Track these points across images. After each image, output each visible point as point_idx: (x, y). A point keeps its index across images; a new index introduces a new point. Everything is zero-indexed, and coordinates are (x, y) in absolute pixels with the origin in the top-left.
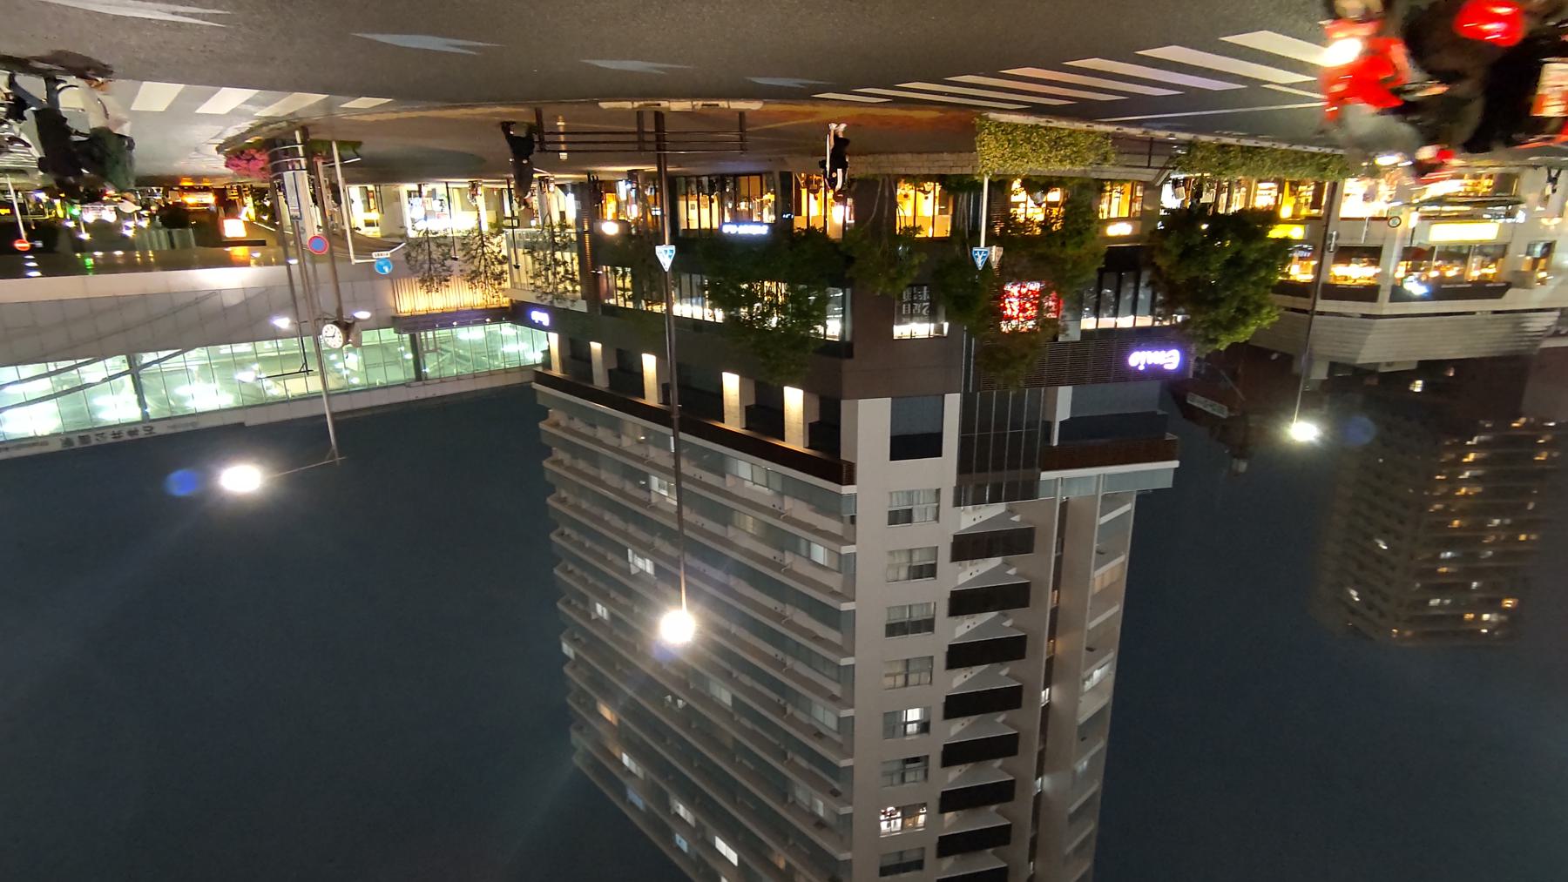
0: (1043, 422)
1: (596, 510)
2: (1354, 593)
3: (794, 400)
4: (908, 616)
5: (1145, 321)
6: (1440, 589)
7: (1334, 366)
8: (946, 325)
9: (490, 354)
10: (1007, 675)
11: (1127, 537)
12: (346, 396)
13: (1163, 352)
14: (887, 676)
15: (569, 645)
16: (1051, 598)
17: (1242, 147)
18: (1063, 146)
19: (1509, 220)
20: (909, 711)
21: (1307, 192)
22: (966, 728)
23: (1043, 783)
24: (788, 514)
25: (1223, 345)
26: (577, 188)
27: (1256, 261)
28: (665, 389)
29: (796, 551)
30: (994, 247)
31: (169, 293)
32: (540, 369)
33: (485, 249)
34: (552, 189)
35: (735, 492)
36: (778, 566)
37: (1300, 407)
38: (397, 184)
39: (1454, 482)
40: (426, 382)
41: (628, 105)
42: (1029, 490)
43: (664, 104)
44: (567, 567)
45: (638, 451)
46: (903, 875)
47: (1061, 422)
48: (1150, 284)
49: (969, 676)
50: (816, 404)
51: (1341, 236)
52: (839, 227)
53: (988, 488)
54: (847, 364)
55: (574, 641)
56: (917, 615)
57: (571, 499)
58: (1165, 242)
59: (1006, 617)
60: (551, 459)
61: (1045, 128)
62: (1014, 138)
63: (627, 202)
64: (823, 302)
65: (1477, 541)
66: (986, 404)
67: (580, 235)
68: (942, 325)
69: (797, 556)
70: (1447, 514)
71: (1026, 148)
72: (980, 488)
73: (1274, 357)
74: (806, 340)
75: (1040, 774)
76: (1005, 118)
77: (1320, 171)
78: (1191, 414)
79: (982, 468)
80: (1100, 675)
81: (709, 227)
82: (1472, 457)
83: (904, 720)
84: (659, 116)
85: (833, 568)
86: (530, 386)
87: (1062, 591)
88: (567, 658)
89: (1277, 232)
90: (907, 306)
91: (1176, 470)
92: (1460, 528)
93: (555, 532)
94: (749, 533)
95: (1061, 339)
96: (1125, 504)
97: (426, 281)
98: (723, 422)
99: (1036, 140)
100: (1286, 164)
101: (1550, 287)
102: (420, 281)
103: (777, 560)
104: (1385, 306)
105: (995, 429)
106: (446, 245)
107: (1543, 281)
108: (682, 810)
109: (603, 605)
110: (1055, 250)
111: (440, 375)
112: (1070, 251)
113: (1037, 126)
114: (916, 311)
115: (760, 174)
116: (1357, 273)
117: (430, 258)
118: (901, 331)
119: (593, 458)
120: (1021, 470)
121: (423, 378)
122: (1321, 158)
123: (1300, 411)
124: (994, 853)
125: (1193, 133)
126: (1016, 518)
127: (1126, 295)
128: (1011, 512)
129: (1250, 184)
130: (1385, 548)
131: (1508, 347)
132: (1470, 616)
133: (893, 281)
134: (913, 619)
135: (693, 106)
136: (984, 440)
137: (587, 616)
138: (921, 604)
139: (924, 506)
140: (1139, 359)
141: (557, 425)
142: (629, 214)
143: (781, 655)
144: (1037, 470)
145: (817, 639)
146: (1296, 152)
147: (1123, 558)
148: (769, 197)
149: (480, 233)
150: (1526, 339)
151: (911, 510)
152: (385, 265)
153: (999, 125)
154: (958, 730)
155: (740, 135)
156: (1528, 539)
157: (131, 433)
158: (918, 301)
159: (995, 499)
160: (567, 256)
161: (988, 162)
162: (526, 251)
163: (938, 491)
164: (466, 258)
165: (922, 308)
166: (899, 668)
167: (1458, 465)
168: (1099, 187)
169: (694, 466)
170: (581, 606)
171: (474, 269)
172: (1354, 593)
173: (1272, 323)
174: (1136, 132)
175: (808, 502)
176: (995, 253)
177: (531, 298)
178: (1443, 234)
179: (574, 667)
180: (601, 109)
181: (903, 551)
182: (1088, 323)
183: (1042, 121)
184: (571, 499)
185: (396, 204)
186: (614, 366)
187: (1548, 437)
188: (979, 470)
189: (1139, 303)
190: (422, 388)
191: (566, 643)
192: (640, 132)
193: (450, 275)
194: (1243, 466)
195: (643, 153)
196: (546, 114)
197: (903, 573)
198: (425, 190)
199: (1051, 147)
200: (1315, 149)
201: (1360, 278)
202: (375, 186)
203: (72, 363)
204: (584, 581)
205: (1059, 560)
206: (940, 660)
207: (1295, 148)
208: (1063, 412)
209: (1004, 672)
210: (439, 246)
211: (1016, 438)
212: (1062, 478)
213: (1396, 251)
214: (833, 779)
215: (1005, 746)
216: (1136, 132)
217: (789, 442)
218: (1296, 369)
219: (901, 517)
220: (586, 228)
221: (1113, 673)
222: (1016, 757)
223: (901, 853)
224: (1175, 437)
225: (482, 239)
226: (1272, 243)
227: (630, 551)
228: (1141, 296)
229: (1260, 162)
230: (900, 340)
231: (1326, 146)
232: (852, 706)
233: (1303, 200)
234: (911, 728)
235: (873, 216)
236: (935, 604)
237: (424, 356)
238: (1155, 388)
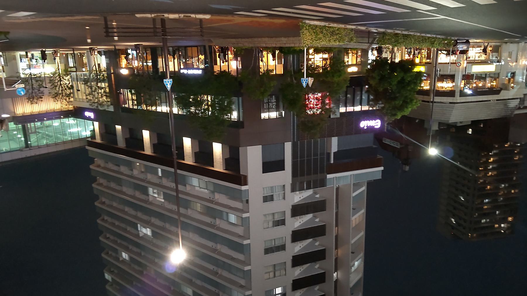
0: (326, 152)
1: (121, 207)
2: (453, 220)
3: (217, 148)
4: (273, 244)
5: (366, 108)
6: (485, 215)
7: (440, 124)
8: (283, 112)
9: (63, 133)
10: (318, 268)
13: (374, 121)
14: (266, 273)
16: (335, 230)
17: (403, 34)
18: (335, 34)
19: (498, 64)
20: (276, 289)
21: (424, 52)
24: (217, 201)
25: (399, 117)
26: (106, 53)
27: (409, 81)
28: (155, 147)
29: (221, 218)
30: (310, 78)
32: (90, 139)
33: (62, 82)
34: (96, 53)
35: (191, 192)
36: (212, 226)
38: (15, 52)
39: (486, 170)
40: (31, 148)
41: (149, 16)
42: (322, 183)
43: (166, 15)
44: (106, 235)
45: (142, 176)
48: (368, 91)
49: (302, 270)
50: (227, 150)
51: (441, 70)
52: (235, 70)
53: (305, 183)
54: (241, 130)
55: (111, 272)
56: (278, 243)
57: (107, 202)
59: (316, 241)
60: (96, 183)
61: (328, 27)
62: (316, 32)
63: (132, 59)
64: (230, 103)
65: (496, 194)
67: (109, 76)
69: (221, 220)
70: (485, 184)
71: (321, 36)
72: (302, 183)
73: (417, 121)
74: (224, 121)
76: (312, 23)
77: (432, 44)
78: (386, 147)
79: (302, 175)
81: (173, 70)
82: (492, 160)
83: (275, 294)
84: (163, 21)
85: (240, 225)
86: (85, 147)
87: (339, 228)
88: (108, 281)
89: (417, 69)
90: (266, 105)
91: (382, 171)
92: (490, 189)
94: (198, 211)
95: (332, 117)
97: (30, 98)
98: (184, 160)
99: (325, 32)
100: (419, 41)
101: (515, 90)
102: (28, 98)
103: (213, 223)
104: (458, 99)
105: (300, 158)
106: (41, 81)
107: (513, 87)
110: (329, 79)
111: (38, 145)
112: (336, 79)
113: (325, 26)
114: (270, 106)
115: (197, 46)
116: (446, 85)
117: (32, 87)
118: (264, 115)
119: (119, 181)
121: (30, 146)
122: (432, 39)
123: (431, 142)
125: (384, 29)
126: (318, 196)
128: (315, 193)
129: (402, 49)
130: (463, 200)
131: (503, 114)
132: (497, 226)
133: (263, 94)
134: (276, 246)
135: (179, 16)
136: (302, 162)
137: (117, 259)
138: (280, 238)
139: (279, 193)
140: (364, 124)
141: (99, 166)
142: (133, 65)
143: (215, 268)
144: (326, 174)
145: (233, 259)
146: (423, 37)
147: (363, 211)
148: (202, 57)
149: (59, 75)
150: (509, 110)
151: (272, 195)
152: (22, 91)
153: (310, 25)
155: (201, 29)
156: (515, 192)
158: (271, 102)
159: (308, 188)
160: (103, 85)
161: (306, 41)
162: (83, 83)
163: (284, 186)
164: (52, 87)
165: (273, 105)
166: (271, 269)
167: (487, 163)
168: (346, 51)
169: (170, 182)
170: (114, 254)
171: (56, 92)
172: (453, 220)
173: (417, 107)
174: (363, 28)
175: (226, 194)
176: (311, 81)
177: (87, 105)
178: (476, 69)
180: (137, 17)
181: (270, 214)
182: (342, 110)
183: (327, 24)
184: (107, 202)
185: (14, 61)
186: (128, 136)
187: (518, 150)
188: (301, 175)
189: (363, 100)
191: (107, 273)
192: (155, 28)
193: (43, 95)
194: (407, 168)
195: (156, 37)
196: (109, 18)
197: (271, 224)
198: (29, 55)
199: (331, 35)
200: (429, 35)
201: (447, 88)
202: (2, 53)
204: (115, 242)
205: (337, 214)
206: (289, 263)
207: (423, 35)
208: (334, 148)
209: (317, 266)
210: (37, 81)
211: (316, 160)
212: (336, 177)
213: (460, 77)
216: (363, 28)
217: (216, 168)
218: (426, 126)
219: (268, 199)
220: (112, 71)
221: (363, 263)
224: (382, 157)
225: (60, 77)
226: (416, 73)
227: (139, 225)
228: (363, 97)
229: (410, 41)
230: (264, 119)
231: (434, 34)
232: (251, 289)
233: (423, 56)
235: (252, 65)
236: (285, 237)
237: (29, 136)
238: (371, 136)
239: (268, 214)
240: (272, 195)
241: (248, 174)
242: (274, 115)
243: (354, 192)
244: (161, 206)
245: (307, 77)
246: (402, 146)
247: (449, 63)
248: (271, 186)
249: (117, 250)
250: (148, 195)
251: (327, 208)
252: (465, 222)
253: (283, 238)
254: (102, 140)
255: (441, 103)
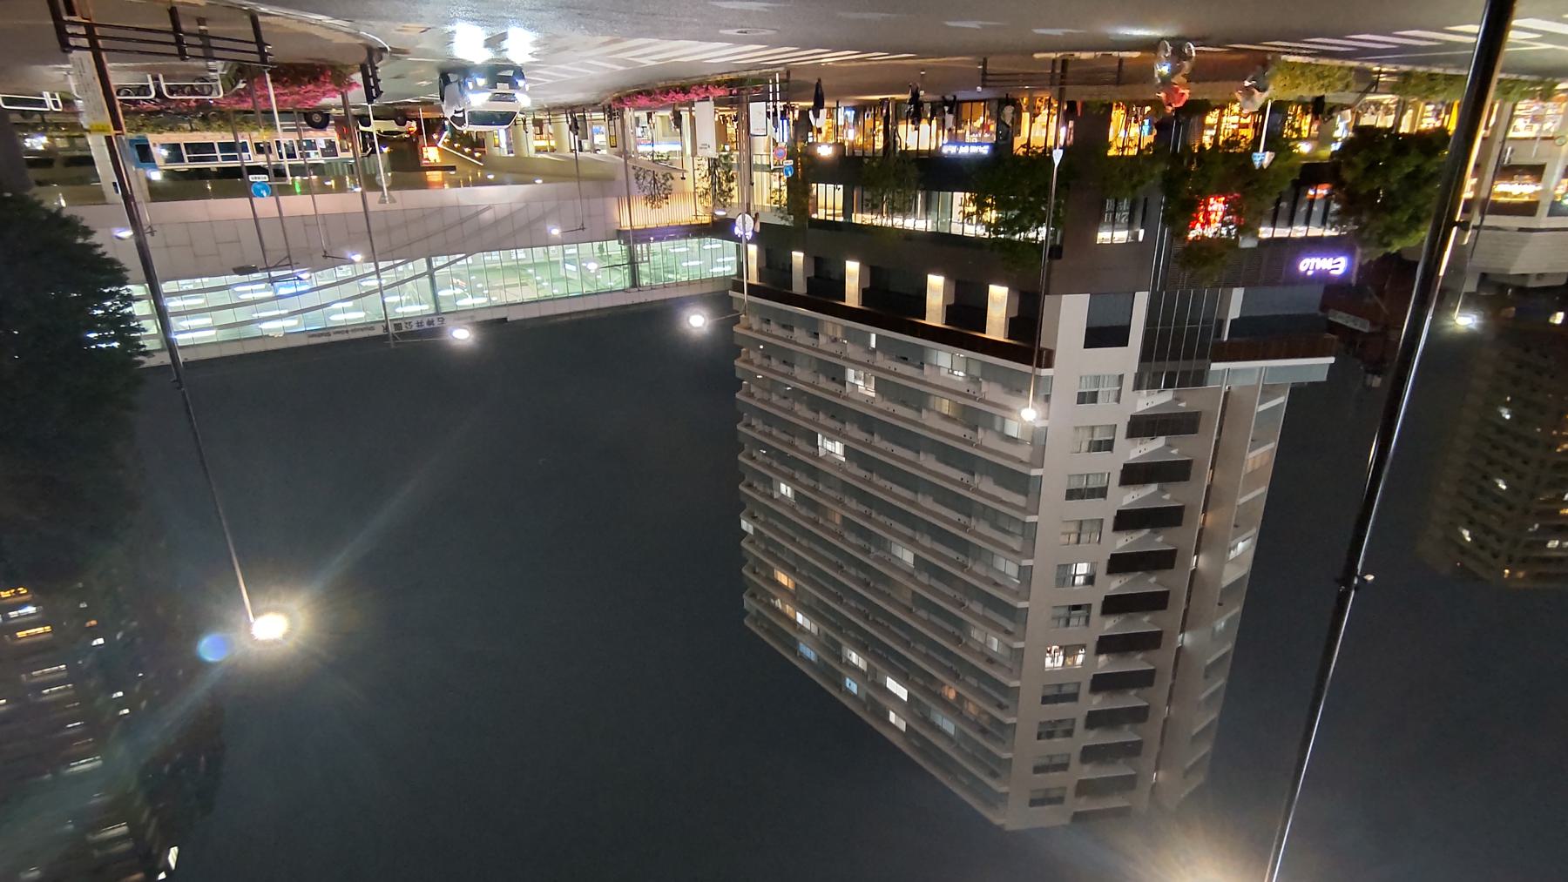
2: (1466, 533)
3: (998, 294)
7: (1484, 278)
8: (1142, 232)
11: (1277, 431)
12: (551, 302)
14: (1063, 534)
15: (747, 522)
17: (1446, 75)
20: (1078, 565)
22: (1122, 586)
23: (1186, 639)
28: (865, 294)
31: (459, 206)
32: (735, 278)
37: (1460, 307)
46: (1061, 705)
47: (1232, 321)
49: (1130, 540)
50: (1016, 300)
58: (1354, 158)
60: (741, 358)
66: (1171, 299)
68: (1138, 232)
72: (1157, 375)
75: (1182, 631)
76: (1292, 59)
79: (1161, 358)
80: (1243, 547)
88: (746, 533)
90: (1108, 216)
91: (1331, 365)
93: (741, 423)
96: (1279, 396)
104: (1542, 220)
108: (854, 658)
109: (787, 485)
115: (984, 101)
120: (1194, 361)
124: (1136, 695)
126: (1183, 405)
127: (1302, 207)
130: (1504, 487)
134: (1089, 487)
138: (1097, 474)
140: (1309, 265)
144: (1208, 360)
147: (1272, 445)
151: (1097, 392)
154: (1116, 585)
157: (419, 324)
159: (1169, 385)
163: (1121, 377)
166: (1073, 528)
179: (752, 542)
181: (1087, 427)
182: (1265, 232)
190: (637, 293)
197: (1085, 446)
203: (391, 263)
208: (1234, 312)
211: (1192, 332)
214: (1008, 614)
215: (1156, 602)
221: (1254, 548)
222: (1164, 611)
223: (1060, 686)
234: (1079, 580)
236: (1109, 474)
238: (1317, 293)
239: (1082, 427)
240: (1097, 392)
241: (1055, 347)
242: (1121, 236)
243: (1260, 404)
244: (868, 402)
245: (1265, 150)
246: (1374, 330)
247: (1535, 138)
248: (1097, 374)
249: (771, 479)
250: (843, 383)
251: (1201, 428)
252: (1499, 540)
253: (1103, 474)
254: (760, 281)
255: (1498, 229)
